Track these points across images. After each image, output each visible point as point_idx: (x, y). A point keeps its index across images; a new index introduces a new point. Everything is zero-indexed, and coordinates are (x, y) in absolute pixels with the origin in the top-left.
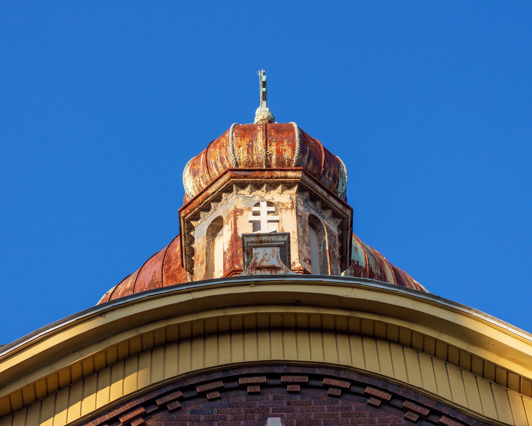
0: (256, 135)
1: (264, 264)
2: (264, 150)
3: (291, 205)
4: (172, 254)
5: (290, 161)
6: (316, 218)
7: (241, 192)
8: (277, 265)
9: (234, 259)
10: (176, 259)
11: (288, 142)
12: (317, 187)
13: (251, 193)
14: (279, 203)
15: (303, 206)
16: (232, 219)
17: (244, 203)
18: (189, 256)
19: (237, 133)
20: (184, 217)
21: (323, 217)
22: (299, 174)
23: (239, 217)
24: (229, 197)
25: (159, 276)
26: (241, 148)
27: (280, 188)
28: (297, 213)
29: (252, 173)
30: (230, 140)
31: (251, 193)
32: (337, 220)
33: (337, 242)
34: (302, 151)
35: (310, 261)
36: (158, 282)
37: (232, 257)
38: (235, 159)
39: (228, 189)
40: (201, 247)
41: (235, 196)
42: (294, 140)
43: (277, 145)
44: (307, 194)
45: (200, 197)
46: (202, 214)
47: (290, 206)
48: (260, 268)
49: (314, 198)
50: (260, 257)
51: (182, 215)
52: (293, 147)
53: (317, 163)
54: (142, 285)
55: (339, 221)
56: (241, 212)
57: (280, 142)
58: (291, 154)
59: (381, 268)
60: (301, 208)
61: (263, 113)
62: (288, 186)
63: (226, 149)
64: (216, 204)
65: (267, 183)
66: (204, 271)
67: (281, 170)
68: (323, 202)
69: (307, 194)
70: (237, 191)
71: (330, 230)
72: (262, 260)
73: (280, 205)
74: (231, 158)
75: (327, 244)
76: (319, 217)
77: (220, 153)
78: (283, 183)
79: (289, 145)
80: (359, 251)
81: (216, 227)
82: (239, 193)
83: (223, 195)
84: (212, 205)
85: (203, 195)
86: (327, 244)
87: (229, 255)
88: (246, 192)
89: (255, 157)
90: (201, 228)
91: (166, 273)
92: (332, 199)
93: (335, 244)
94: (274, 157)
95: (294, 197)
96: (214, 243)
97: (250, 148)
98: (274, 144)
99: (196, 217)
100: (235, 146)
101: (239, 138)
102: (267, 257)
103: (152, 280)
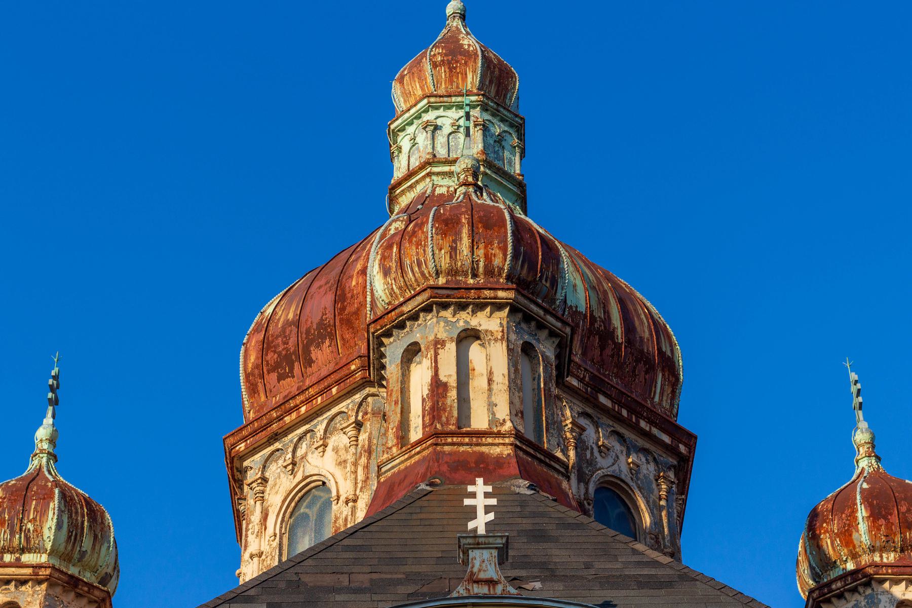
0: (460, 232)
1: (482, 576)
2: (470, 254)
3: (501, 334)
4: (347, 289)
5: (501, 269)
6: (530, 343)
7: (443, 313)
8: (495, 578)
9: (435, 413)
10: (352, 297)
11: (498, 243)
12: (533, 307)
13: (454, 316)
14: (487, 331)
15: (517, 333)
16: (432, 352)
17: (446, 331)
18: (378, 370)
19: (437, 228)
20: (373, 333)
21: (538, 340)
22: (511, 295)
23: (440, 351)
24: (428, 318)
25: (330, 316)
26: (443, 251)
27: (488, 309)
28: (508, 346)
29: (456, 291)
30: (430, 239)
31: (454, 316)
32: (554, 339)
33: (554, 371)
34: (515, 256)
35: (522, 413)
36: (329, 325)
37: (433, 408)
38: (436, 266)
39: (428, 309)
40: (395, 378)
41: (435, 320)
42: (506, 242)
43: (486, 247)
44: (520, 315)
45: (393, 313)
46: (395, 332)
47: (499, 336)
48: (478, 582)
49: (528, 318)
50: (477, 564)
51: (372, 330)
52: (505, 255)
53: (532, 268)
54: (309, 323)
55: (557, 341)
56: (443, 343)
57: (488, 244)
58: (503, 261)
59: (604, 307)
60: (513, 337)
61: (466, 161)
62: (499, 307)
63: (424, 251)
64: (412, 323)
65: (474, 304)
66: (399, 415)
67: (490, 289)
68: (538, 321)
69: (520, 315)
70: (438, 312)
71: (547, 357)
72: (480, 571)
73: (489, 334)
74: (431, 265)
75: (542, 380)
76: (534, 342)
77: (418, 253)
78: (492, 304)
79: (500, 248)
80: (578, 288)
81: (412, 352)
82: (440, 315)
83: (421, 315)
84: (408, 323)
85: (397, 311)
86: (542, 380)
87: (429, 405)
88: (447, 314)
89: (459, 264)
90: (394, 349)
91: (340, 314)
92: (549, 318)
93: (551, 376)
94: (481, 264)
95: (505, 323)
96: (409, 371)
97: (453, 251)
98: (482, 246)
99: (388, 334)
100: (435, 248)
101: (439, 237)
102: (484, 565)
103: (322, 319)
